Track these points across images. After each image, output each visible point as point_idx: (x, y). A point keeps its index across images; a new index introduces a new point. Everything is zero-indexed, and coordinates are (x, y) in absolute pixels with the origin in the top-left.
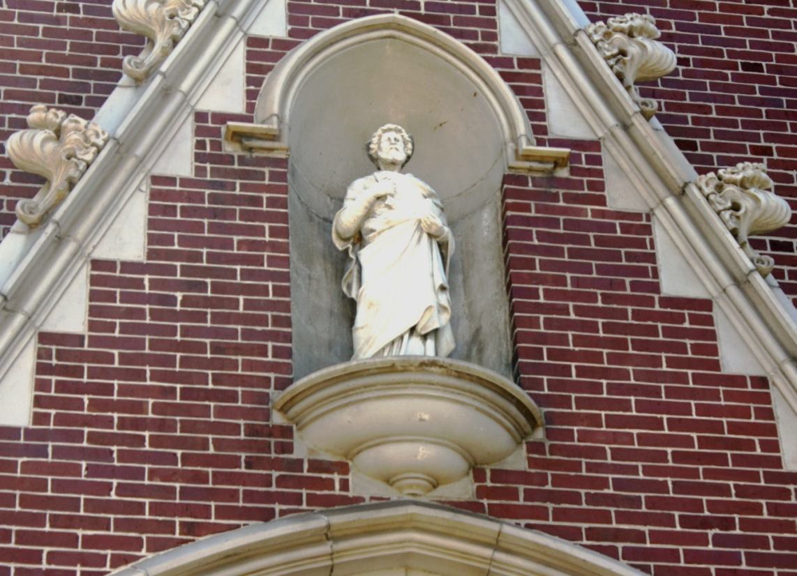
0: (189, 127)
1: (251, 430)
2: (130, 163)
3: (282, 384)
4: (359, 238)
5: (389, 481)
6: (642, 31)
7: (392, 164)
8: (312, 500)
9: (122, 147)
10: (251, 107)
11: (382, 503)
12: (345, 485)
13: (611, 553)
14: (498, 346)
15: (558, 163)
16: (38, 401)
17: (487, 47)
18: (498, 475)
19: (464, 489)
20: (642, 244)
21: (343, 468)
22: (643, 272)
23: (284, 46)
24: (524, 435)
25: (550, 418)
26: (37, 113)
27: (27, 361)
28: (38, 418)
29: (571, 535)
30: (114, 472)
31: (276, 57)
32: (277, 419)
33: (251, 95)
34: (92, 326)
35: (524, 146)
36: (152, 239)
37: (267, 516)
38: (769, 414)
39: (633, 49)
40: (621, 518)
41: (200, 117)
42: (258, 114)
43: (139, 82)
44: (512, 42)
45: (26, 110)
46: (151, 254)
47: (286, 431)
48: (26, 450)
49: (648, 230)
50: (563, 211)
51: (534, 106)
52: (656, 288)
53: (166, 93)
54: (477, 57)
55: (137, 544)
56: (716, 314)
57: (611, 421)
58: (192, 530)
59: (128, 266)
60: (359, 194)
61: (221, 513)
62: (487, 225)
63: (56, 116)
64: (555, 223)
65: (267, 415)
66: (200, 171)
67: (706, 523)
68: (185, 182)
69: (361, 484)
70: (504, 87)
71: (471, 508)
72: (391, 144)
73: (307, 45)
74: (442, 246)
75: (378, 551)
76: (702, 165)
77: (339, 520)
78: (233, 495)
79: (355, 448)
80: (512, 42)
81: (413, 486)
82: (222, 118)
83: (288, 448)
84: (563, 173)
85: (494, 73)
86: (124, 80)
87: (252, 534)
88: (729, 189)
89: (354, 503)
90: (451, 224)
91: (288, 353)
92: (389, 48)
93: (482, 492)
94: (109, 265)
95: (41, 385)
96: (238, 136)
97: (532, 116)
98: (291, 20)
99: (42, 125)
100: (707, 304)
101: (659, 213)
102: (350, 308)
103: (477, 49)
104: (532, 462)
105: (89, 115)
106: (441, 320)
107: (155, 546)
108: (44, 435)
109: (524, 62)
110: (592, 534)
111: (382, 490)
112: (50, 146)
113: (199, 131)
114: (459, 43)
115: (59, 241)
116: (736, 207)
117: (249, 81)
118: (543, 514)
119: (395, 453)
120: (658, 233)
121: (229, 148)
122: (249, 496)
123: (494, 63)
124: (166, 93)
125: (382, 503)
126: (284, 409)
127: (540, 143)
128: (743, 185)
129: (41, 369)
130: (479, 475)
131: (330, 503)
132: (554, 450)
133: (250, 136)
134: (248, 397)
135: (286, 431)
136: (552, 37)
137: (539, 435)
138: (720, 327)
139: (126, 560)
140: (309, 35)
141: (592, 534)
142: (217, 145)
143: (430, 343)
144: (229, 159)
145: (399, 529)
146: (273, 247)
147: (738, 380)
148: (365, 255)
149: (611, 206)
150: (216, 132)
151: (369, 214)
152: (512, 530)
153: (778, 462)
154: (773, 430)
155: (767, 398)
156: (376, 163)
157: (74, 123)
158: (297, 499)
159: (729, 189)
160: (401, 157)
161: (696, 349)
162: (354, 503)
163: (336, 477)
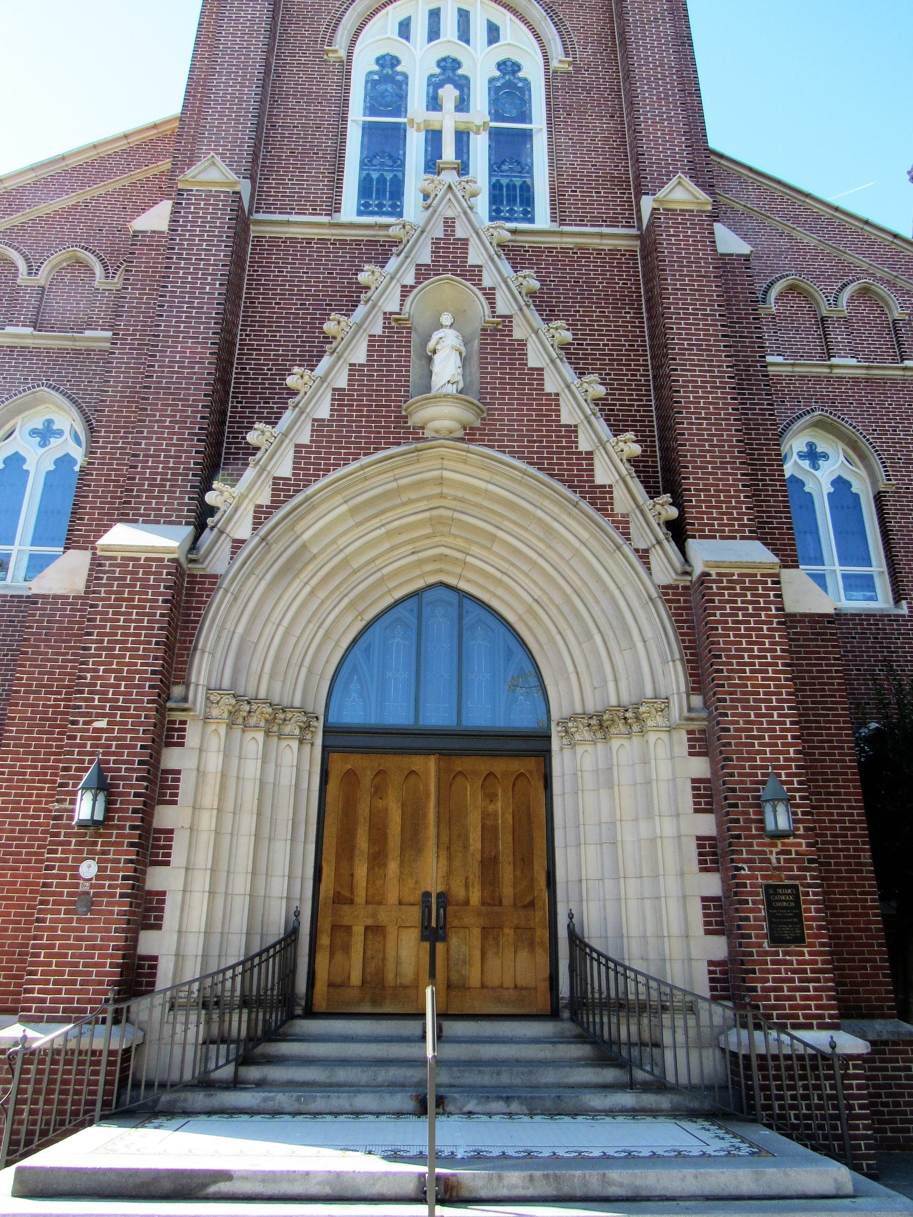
0: (381, 316)
1: (396, 417)
2: (362, 331)
3: (405, 401)
4: (434, 352)
5: (437, 432)
6: (529, 276)
7: (446, 326)
8: (413, 439)
9: (359, 326)
10: (401, 309)
11: (435, 439)
12: (423, 433)
13: (504, 452)
14: (476, 386)
15: (498, 324)
16: (332, 410)
17: (478, 285)
18: (471, 429)
19: (460, 434)
20: (523, 350)
21: (423, 428)
22: (523, 359)
23: (413, 287)
24: (479, 415)
25: (489, 409)
26: (333, 315)
27: (329, 397)
28: (332, 415)
29: (492, 447)
30: (353, 432)
31: (410, 292)
32: (404, 413)
33: (402, 305)
34: (349, 385)
35: (487, 319)
36: (368, 356)
37: (399, 444)
38: (558, 405)
39: (525, 283)
40: (508, 441)
41: (385, 313)
42: (403, 312)
43: (367, 302)
44: (487, 282)
45: (329, 315)
46: (368, 361)
47: (406, 417)
48: (327, 426)
49: (525, 345)
50: (499, 340)
51: (492, 304)
52: (526, 364)
53: (374, 307)
54: (474, 289)
55: (359, 454)
56: (545, 373)
57: (508, 410)
58: (376, 449)
59: (360, 365)
60: (436, 336)
61: (386, 443)
62: (476, 344)
63: (338, 317)
64: (496, 344)
65: (400, 412)
66: (384, 332)
67: (535, 442)
68: (379, 336)
69: (428, 433)
70: (482, 298)
71: (461, 440)
72: (446, 319)
73: (420, 286)
74: (460, 354)
75: (338, 587)
76: (547, 320)
77: (420, 445)
78: (389, 438)
79: (426, 423)
80: (487, 282)
81: (444, 433)
82: (391, 313)
83: (406, 422)
84: (500, 327)
85: (479, 294)
86: (362, 302)
87: (395, 450)
88: (552, 330)
89: (425, 439)
90: (465, 344)
91: (408, 391)
92: (446, 286)
93: (466, 434)
94: (354, 365)
95: (333, 405)
96: (396, 320)
97: (492, 307)
98: (416, 278)
99: (333, 320)
100: (542, 369)
101: (530, 339)
102: (431, 373)
103: (474, 285)
104: (482, 424)
105: (348, 316)
106: (460, 378)
107: (365, 454)
108: (333, 421)
109: (490, 289)
110: (499, 446)
111: (434, 435)
112: (336, 327)
113: (385, 319)
114: (468, 283)
115: (339, 358)
116: (553, 337)
117: (401, 300)
118: (483, 440)
119: (437, 424)
120: (528, 345)
121: (393, 324)
122: (394, 438)
123: (480, 289)
124: (374, 307)
125: (435, 439)
126: (406, 410)
127: (493, 317)
128: (557, 329)
129: (333, 400)
130: (465, 429)
131: (418, 439)
132: (489, 420)
133: (399, 320)
134: (395, 406)
135: (406, 417)
136: (500, 280)
137: (485, 415)
138: (546, 377)
139: (356, 459)
140: (421, 283)
141: (499, 446)
142: (389, 323)
143: (455, 386)
144: (393, 328)
145: (438, 447)
146: (406, 356)
147: (550, 394)
148: (436, 357)
149: (457, 236)
150: (390, 319)
151: (438, 343)
152: (473, 447)
153: (593, 481)
154: (559, 411)
155: (558, 400)
156: (442, 326)
157: (343, 319)
158: (408, 438)
159: (552, 330)
160: (449, 324)
161: (537, 384)
162: (425, 439)
163: (421, 431)
